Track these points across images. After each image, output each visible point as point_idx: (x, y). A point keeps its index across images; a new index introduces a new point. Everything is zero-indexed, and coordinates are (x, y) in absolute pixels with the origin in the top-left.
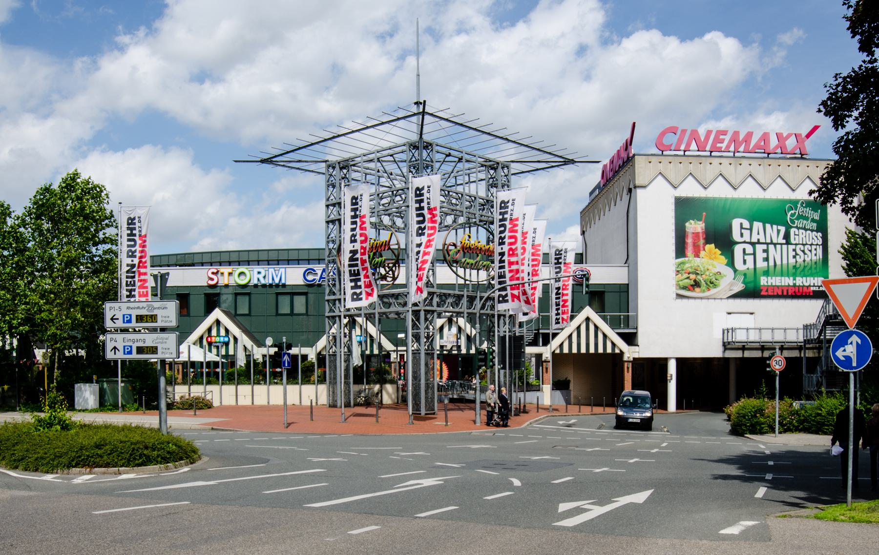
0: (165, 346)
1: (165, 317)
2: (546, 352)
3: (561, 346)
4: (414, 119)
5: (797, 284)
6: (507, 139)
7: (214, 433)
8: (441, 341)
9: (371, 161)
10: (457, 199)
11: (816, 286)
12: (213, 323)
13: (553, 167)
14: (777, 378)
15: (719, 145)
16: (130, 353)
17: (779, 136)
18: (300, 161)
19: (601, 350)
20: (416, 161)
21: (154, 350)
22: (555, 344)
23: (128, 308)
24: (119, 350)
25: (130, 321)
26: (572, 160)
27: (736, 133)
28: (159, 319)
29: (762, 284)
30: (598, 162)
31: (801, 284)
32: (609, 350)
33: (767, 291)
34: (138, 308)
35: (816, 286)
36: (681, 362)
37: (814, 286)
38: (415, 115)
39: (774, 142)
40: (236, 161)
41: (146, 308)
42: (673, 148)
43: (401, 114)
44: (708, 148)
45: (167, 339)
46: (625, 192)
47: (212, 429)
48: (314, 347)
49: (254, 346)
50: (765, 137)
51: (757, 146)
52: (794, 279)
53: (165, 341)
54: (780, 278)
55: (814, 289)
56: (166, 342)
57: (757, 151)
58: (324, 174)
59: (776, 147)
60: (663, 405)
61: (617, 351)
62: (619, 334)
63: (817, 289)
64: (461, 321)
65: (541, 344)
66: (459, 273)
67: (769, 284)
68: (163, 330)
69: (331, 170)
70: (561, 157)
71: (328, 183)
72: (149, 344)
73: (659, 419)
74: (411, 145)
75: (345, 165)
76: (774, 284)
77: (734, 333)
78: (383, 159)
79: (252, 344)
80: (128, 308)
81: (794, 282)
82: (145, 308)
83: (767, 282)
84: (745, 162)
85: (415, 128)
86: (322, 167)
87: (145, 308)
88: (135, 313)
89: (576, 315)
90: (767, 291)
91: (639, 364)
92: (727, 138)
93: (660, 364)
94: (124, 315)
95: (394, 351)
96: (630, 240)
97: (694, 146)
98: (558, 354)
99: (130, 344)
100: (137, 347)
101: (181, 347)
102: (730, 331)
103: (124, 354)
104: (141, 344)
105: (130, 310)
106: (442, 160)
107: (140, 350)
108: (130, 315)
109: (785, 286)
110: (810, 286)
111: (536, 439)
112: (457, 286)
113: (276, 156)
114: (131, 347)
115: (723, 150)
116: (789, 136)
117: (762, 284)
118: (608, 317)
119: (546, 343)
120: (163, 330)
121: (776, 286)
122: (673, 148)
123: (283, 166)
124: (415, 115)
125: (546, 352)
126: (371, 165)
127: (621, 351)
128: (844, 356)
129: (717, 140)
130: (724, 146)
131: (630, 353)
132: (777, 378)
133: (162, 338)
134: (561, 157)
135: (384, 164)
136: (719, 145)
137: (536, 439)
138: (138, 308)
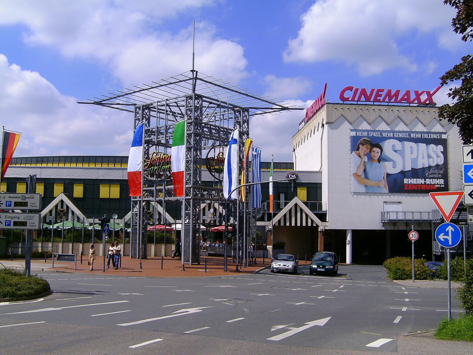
0: (31, 221)
1: (33, 203)
2: (269, 225)
3: (279, 221)
4: (191, 81)
5: (427, 183)
6: (247, 95)
7: (58, 274)
8: (204, 217)
9: (163, 105)
10: (215, 130)
11: (439, 184)
12: (59, 202)
13: (275, 111)
14: (413, 245)
15: (378, 98)
16: (9, 225)
17: (416, 93)
18: (119, 104)
19: (304, 224)
20: (191, 107)
21: (24, 224)
22: (275, 220)
23: (9, 197)
24: (2, 223)
25: (10, 205)
26: (287, 107)
27: (389, 91)
28: (29, 204)
29: (405, 183)
30: (303, 109)
31: (429, 183)
32: (309, 224)
33: (408, 187)
34: (16, 197)
35: (439, 184)
36: (355, 233)
37: (437, 184)
38: (191, 79)
39: (413, 96)
40: (78, 103)
41: (21, 198)
42: (350, 99)
43: (182, 78)
44: (372, 100)
45: (33, 217)
46: (320, 125)
47: (57, 272)
48: (123, 219)
49: (85, 217)
50: (408, 93)
51: (403, 99)
52: (425, 180)
53: (32, 218)
54: (416, 179)
55: (438, 186)
56: (32, 219)
57: (402, 102)
58: (133, 112)
59: (414, 100)
60: (344, 260)
61: (314, 225)
62: (315, 214)
63: (439, 186)
64: (216, 205)
65: (266, 220)
66: (216, 176)
67: (410, 183)
68: (31, 211)
69: (138, 110)
70: (280, 106)
71: (136, 118)
72: (22, 220)
73: (341, 269)
74: (188, 97)
75: (148, 107)
76: (412, 183)
77: (388, 215)
78: (170, 104)
79: (84, 216)
80: (9, 197)
81: (425, 182)
82: (20, 198)
83: (408, 182)
84: (395, 109)
85: (191, 87)
86: (132, 108)
87: (20, 198)
88: (13, 200)
89: (289, 202)
90: (408, 187)
91: (327, 233)
92: (384, 94)
93: (341, 234)
94: (7, 202)
95: (174, 223)
96: (323, 156)
97: (363, 98)
98: (277, 226)
99: (10, 219)
100: (14, 222)
101: (19, 210)
102: (386, 213)
103: (6, 225)
104: (16, 220)
105: (11, 199)
106: (207, 106)
107: (16, 224)
108: (11, 202)
109: (419, 184)
110: (435, 184)
111: (261, 282)
112: (214, 182)
113: (104, 100)
114: (10, 221)
115: (381, 101)
116: (423, 92)
117: (405, 183)
118: (309, 203)
119: (270, 219)
120: (31, 211)
121: (413, 184)
122: (350, 99)
123: (108, 106)
124: (191, 79)
125: (269, 225)
126: (163, 108)
127: (317, 225)
128: (448, 230)
129: (378, 95)
130: (381, 98)
131: (322, 226)
132: (413, 245)
133: (30, 217)
134: (280, 106)
135: (171, 107)
136: (378, 98)
137: (261, 282)
138: (16, 197)
